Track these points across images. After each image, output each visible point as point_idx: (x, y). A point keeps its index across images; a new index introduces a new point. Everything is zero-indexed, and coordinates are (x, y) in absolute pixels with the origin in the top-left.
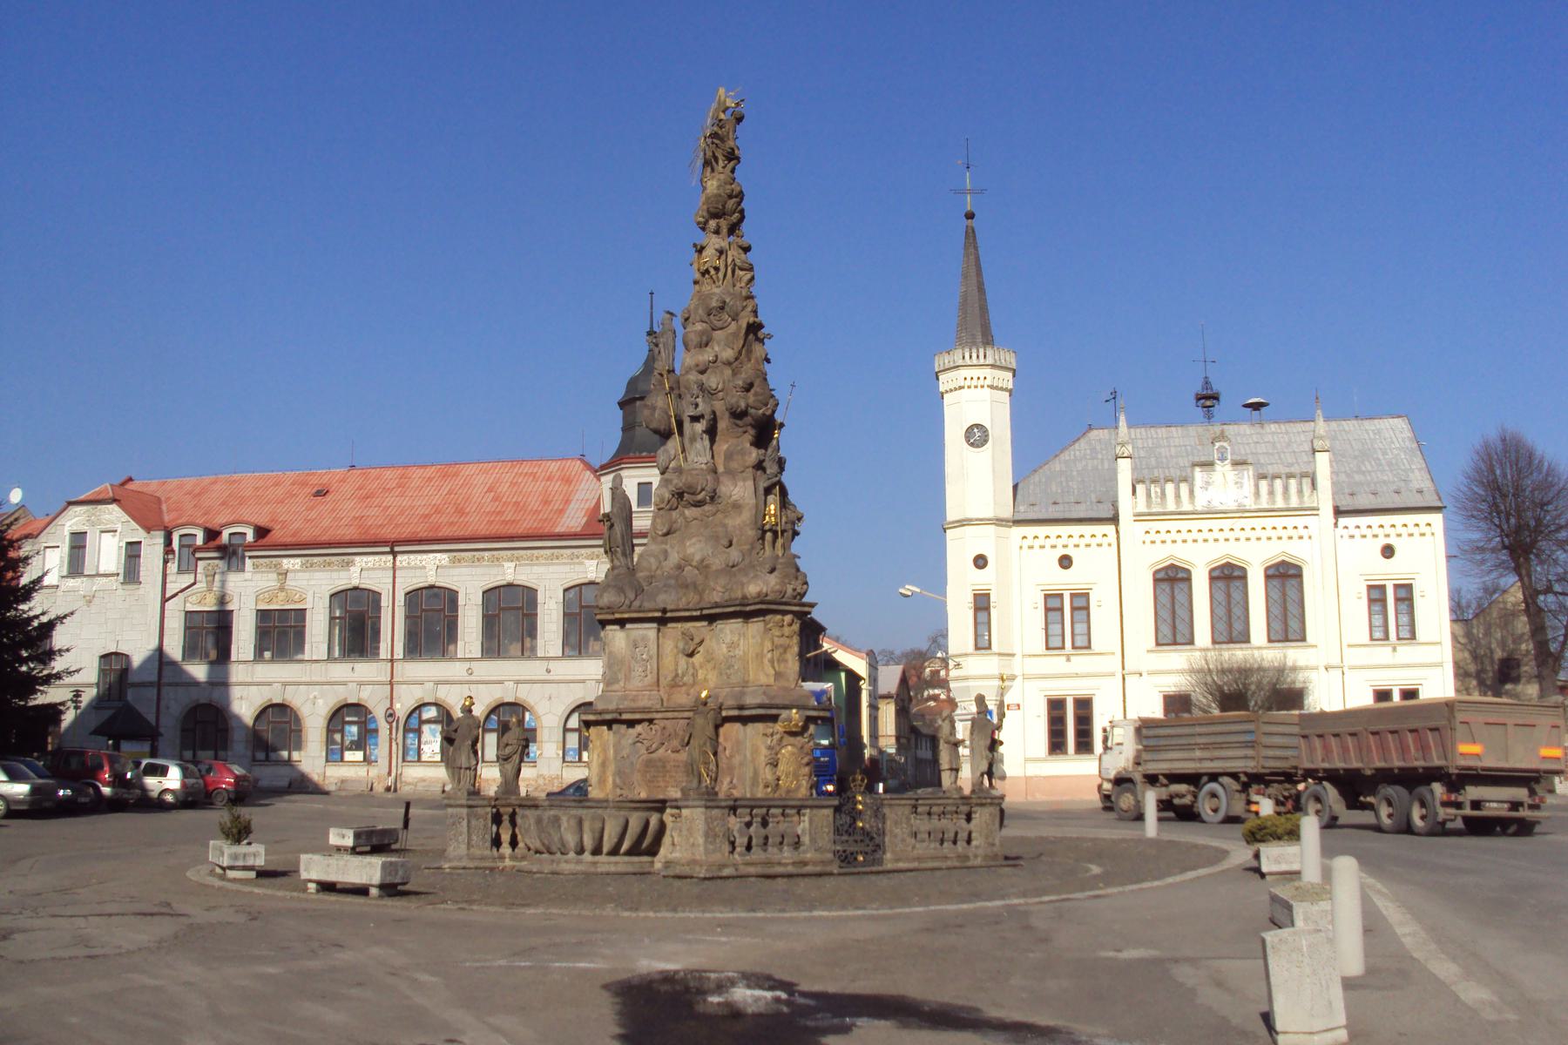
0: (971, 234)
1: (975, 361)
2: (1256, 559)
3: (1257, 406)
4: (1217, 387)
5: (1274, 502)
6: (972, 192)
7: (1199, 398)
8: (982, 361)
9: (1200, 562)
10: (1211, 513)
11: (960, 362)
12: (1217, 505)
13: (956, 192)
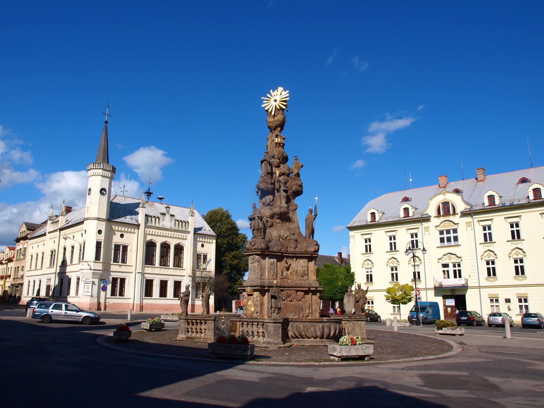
2: (173, 243)
8: (99, 167)
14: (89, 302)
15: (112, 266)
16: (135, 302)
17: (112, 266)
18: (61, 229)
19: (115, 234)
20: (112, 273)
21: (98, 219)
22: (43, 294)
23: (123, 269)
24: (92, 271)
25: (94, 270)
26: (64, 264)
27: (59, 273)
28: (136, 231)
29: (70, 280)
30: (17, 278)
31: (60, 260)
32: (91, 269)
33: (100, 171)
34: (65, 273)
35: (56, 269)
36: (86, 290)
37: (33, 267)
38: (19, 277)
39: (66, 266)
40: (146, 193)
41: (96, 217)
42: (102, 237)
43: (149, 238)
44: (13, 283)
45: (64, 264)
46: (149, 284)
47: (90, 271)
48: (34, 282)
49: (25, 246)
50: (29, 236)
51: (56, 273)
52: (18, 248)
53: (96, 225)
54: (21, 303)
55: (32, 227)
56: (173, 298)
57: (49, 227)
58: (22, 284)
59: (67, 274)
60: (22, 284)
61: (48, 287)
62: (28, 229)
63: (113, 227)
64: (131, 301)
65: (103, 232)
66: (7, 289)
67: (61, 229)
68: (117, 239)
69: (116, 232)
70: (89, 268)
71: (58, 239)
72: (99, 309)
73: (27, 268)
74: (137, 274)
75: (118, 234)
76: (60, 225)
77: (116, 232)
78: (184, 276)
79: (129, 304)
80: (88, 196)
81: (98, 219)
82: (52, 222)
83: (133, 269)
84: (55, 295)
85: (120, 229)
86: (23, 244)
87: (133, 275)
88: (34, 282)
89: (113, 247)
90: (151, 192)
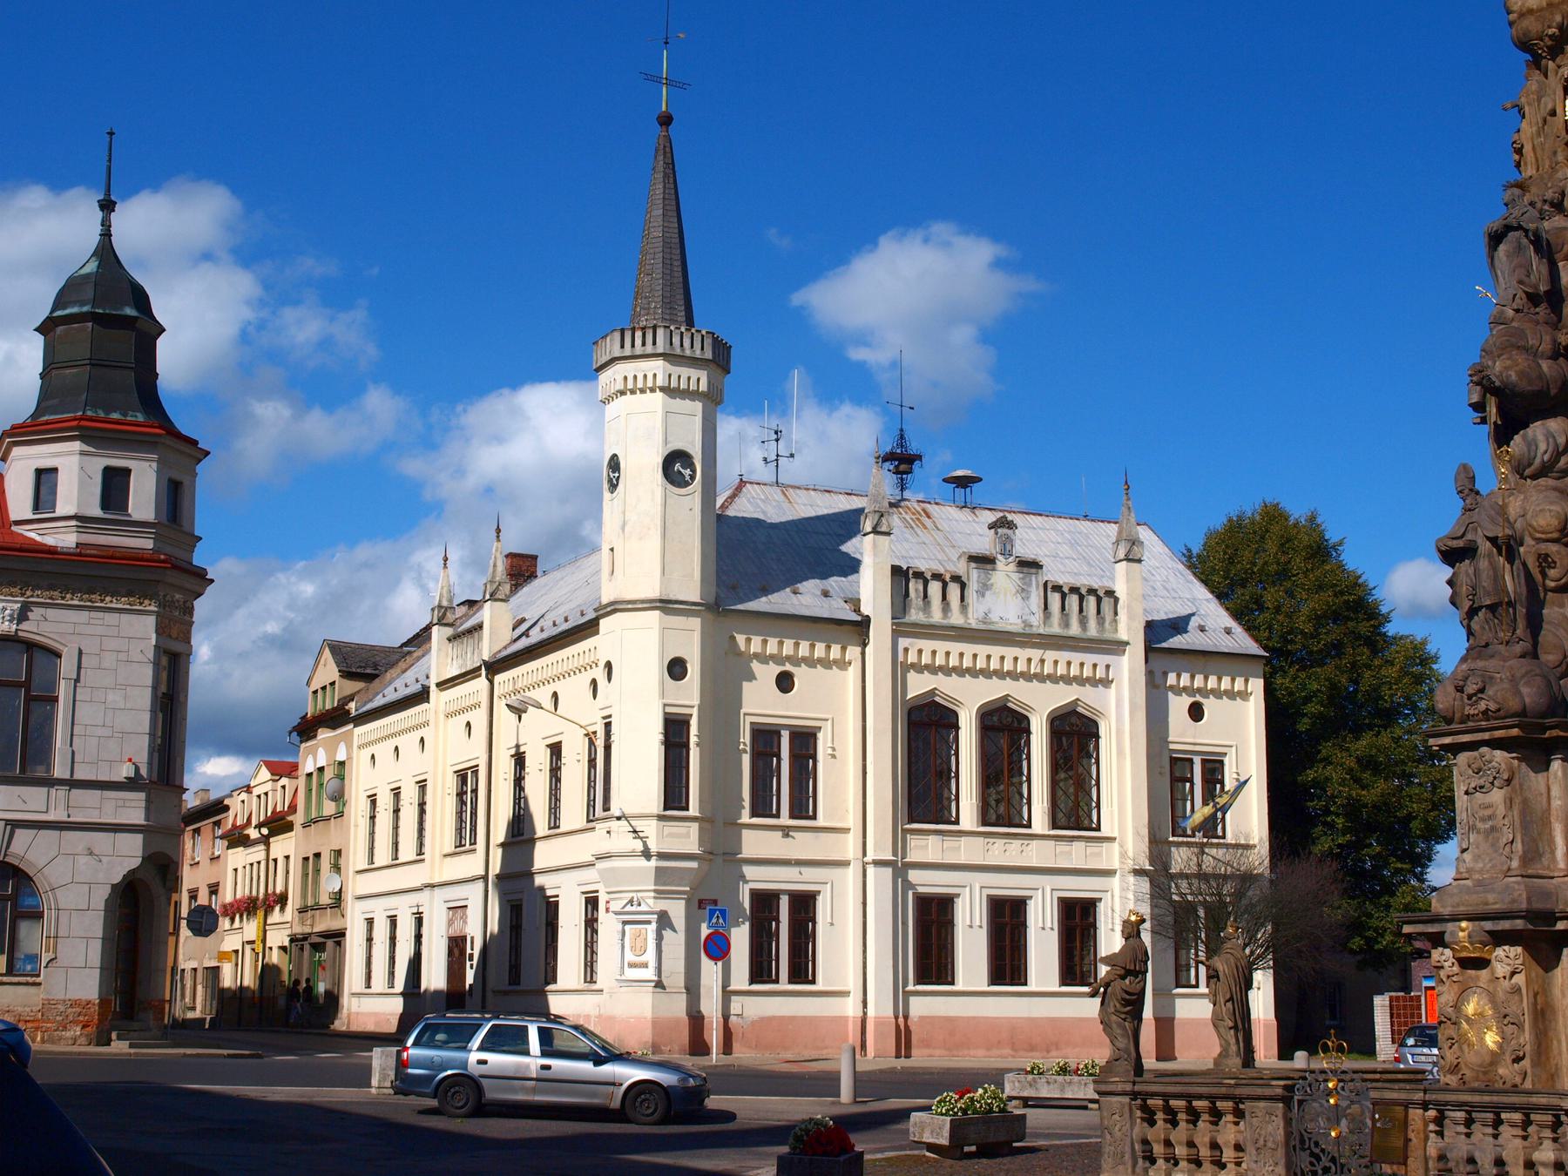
0: (667, 151)
1: (639, 350)
2: (1040, 705)
3: (963, 482)
4: (914, 447)
5: (1067, 625)
6: (670, 83)
7: (888, 457)
8: (649, 349)
9: (969, 700)
11: (617, 352)
13: (682, 86)
15: (745, 833)
16: (871, 1012)
17: (745, 833)
18: (495, 667)
19: (751, 677)
20: (749, 871)
21: (665, 605)
22: (435, 977)
23: (803, 845)
24: (653, 863)
25: (662, 856)
26: (520, 833)
28: (853, 652)
32: (646, 854)
33: (657, 368)
34: (530, 875)
36: (629, 957)
38: (325, 899)
43: (918, 685)
45: (520, 833)
47: (643, 862)
48: (393, 921)
51: (485, 878)
52: (309, 766)
53: (653, 637)
54: (339, 1025)
55: (363, 665)
58: (338, 936)
61: (457, 946)
62: (347, 674)
63: (741, 639)
66: (275, 957)
67: (495, 667)
68: (760, 701)
69: (755, 665)
70: (639, 845)
72: (698, 1046)
73: (356, 857)
75: (766, 674)
76: (488, 647)
77: (755, 665)
78: (1109, 873)
79: (843, 1020)
80: (607, 495)
81: (665, 605)
82: (449, 631)
83: (849, 847)
84: (491, 984)
86: (331, 748)
87: (851, 875)
88: (393, 921)
89: (746, 738)
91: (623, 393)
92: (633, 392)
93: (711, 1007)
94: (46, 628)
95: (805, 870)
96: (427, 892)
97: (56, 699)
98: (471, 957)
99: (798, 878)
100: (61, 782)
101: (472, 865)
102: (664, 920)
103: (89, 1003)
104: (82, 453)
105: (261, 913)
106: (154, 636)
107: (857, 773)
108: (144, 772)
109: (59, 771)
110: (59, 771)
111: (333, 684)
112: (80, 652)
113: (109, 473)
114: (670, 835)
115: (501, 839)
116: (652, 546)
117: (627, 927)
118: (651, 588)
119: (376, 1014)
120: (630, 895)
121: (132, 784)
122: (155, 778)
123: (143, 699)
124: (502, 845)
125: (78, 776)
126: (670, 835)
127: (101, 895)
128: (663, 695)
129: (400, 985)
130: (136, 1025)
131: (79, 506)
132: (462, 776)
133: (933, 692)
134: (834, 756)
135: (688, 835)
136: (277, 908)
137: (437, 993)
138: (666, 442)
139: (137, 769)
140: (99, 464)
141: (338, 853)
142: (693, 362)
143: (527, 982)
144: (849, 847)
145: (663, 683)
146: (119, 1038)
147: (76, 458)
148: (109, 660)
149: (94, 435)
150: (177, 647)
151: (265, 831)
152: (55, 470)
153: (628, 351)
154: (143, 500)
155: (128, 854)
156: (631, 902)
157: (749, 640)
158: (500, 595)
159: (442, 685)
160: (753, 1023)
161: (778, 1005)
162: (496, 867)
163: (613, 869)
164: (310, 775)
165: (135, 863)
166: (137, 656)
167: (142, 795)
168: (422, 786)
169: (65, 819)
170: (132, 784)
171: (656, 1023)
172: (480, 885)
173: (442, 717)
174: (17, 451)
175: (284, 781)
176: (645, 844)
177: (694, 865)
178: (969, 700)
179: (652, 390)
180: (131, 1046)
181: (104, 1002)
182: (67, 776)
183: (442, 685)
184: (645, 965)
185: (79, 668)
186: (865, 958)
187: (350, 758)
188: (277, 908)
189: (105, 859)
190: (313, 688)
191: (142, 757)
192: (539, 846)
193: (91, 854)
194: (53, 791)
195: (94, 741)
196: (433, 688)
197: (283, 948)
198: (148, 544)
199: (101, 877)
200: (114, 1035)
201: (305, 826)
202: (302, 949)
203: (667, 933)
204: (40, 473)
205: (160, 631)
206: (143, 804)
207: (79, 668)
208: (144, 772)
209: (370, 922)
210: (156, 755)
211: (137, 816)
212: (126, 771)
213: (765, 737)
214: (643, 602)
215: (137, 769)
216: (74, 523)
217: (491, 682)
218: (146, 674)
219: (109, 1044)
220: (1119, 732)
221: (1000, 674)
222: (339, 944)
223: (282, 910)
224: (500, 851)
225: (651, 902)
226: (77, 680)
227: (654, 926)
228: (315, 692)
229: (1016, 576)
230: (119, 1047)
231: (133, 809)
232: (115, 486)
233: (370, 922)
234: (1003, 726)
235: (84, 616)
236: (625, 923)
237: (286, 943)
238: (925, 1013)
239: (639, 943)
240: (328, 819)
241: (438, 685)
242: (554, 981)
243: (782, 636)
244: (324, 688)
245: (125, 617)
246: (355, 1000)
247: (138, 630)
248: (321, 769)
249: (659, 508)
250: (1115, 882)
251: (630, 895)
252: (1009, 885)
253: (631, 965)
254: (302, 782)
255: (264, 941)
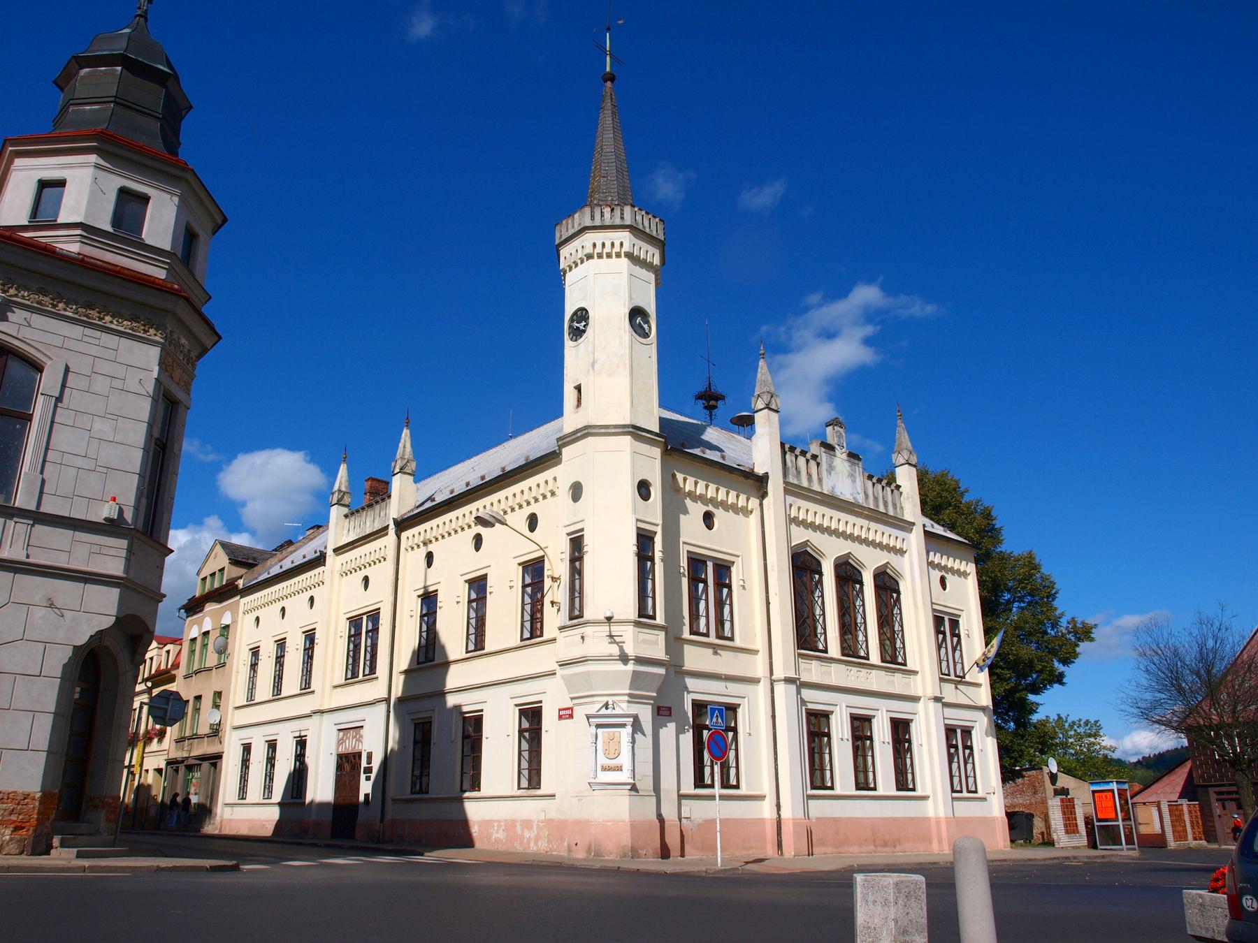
2: (869, 562)
4: (719, 388)
8: (618, 221)
10: (832, 501)
11: (588, 222)
12: (838, 493)
14: (625, 816)
15: (687, 647)
16: (786, 813)
17: (687, 647)
18: (403, 524)
19: (686, 512)
20: (691, 683)
21: (635, 431)
22: (321, 788)
23: (725, 663)
24: (631, 667)
25: (640, 661)
26: (430, 656)
27: (400, 700)
28: (754, 503)
29: (472, 727)
30: (195, 737)
31: (409, 639)
32: (624, 658)
33: (625, 237)
34: (442, 694)
35: (390, 679)
36: (602, 760)
37: (264, 689)
38: (204, 729)
39: (446, 664)
40: (699, 397)
41: (627, 421)
42: (654, 511)
43: (800, 536)
44: (174, 754)
45: (430, 656)
46: (816, 727)
47: (619, 666)
48: (272, 745)
49: (227, 619)
50: (241, 583)
51: (387, 700)
52: (194, 632)
53: (626, 457)
54: (209, 829)
55: (243, 559)
56: (895, 793)
57: (339, 529)
58: (215, 760)
59: (451, 701)
60: (219, 756)
61: (348, 765)
62: (235, 562)
63: (680, 477)
64: (766, 810)
65: (656, 492)
66: (150, 779)
67: (403, 524)
68: (692, 532)
69: (688, 502)
70: (615, 650)
71: (389, 566)
72: (665, 852)
73: (237, 695)
74: (780, 688)
75: (696, 510)
76: (396, 507)
77: (688, 502)
78: (915, 699)
79: (760, 822)
80: (568, 343)
81: (635, 431)
82: (346, 510)
83: (758, 667)
84: (392, 792)
85: (700, 489)
86: (217, 616)
87: (762, 690)
88: (272, 745)
89: (684, 563)
90: (700, 402)
91: (589, 257)
92: (600, 256)
93: (669, 812)
94: (26, 333)
95: (731, 685)
96: (316, 718)
97: (29, 418)
98: (368, 770)
99: (730, 692)
100: (23, 513)
101: (376, 689)
102: (637, 726)
103: (26, 796)
104: (97, 166)
105: (141, 745)
106: (156, 369)
107: (760, 603)
108: (128, 516)
109: (23, 498)
110: (23, 498)
111: (222, 570)
112: (67, 370)
113: (123, 192)
114: (644, 641)
115: (404, 666)
116: (623, 380)
117: (600, 731)
118: (623, 417)
119: (249, 821)
120: (605, 699)
121: (112, 527)
122: (140, 526)
123: (137, 434)
124: (406, 672)
125: (46, 508)
126: (644, 641)
127: (59, 658)
128: (635, 510)
129: (277, 796)
130: (84, 827)
131: (86, 216)
132: (355, 622)
133: (806, 543)
134: (744, 588)
135: (656, 643)
136: (156, 740)
137: (323, 805)
138: (631, 298)
139: (121, 511)
140: (114, 182)
141: (218, 695)
142: (650, 239)
143: (437, 787)
144: (760, 670)
145: (634, 500)
146: (63, 845)
147: (91, 170)
148: (100, 385)
149: (113, 147)
150: (179, 394)
151: (149, 684)
152: (61, 183)
153: (598, 222)
154: (161, 220)
155: (98, 610)
156: (606, 706)
157: (685, 480)
158: (408, 470)
159: (339, 550)
160: (699, 825)
161: (712, 810)
162: (397, 691)
163: (588, 673)
164: (194, 640)
165: (107, 622)
166: (133, 385)
167: (124, 543)
168: (310, 637)
169: (24, 559)
170: (112, 527)
171: (634, 826)
172: (383, 706)
173: (337, 576)
174: (19, 162)
175: (169, 647)
176: (621, 649)
177: (662, 671)
178: (829, 552)
179: (618, 255)
180: (80, 855)
181: (46, 796)
182: (33, 508)
183: (339, 550)
184: (619, 769)
185: (64, 386)
186: (776, 765)
187: (235, 621)
188: (156, 740)
189: (68, 614)
190: (202, 576)
191: (129, 497)
192: (453, 669)
193: (51, 605)
194: (11, 524)
195: (71, 472)
196: (330, 552)
197: (159, 771)
198: (161, 274)
199: (61, 636)
200: (56, 841)
201: (186, 677)
202: (177, 771)
203: (639, 736)
204: (43, 185)
205: (163, 363)
206: (124, 554)
207: (64, 386)
208: (128, 516)
209: (247, 748)
210: (144, 501)
211: (115, 567)
212: (106, 511)
213: (697, 563)
214: (616, 427)
215: (121, 511)
216: (78, 232)
217: (399, 537)
218: (143, 409)
219: (48, 853)
220: (914, 590)
221: (851, 537)
222: (215, 765)
223: (160, 741)
224: (402, 677)
225: (624, 705)
226: (59, 399)
227: (629, 729)
228: (204, 579)
229: (847, 464)
230: (62, 857)
231: (111, 557)
232: (130, 207)
233: (247, 748)
234: (848, 574)
235: (77, 331)
236: (598, 726)
237: (163, 765)
238: (819, 815)
239: (613, 746)
240: (210, 669)
241: (335, 550)
242: (476, 784)
243: (709, 480)
244: (213, 575)
245: (125, 343)
246: (228, 810)
247: (139, 361)
248: (206, 634)
249: (627, 350)
250: (920, 706)
251: (605, 699)
252: (863, 705)
253: (604, 769)
254: (186, 645)
255: (141, 765)
